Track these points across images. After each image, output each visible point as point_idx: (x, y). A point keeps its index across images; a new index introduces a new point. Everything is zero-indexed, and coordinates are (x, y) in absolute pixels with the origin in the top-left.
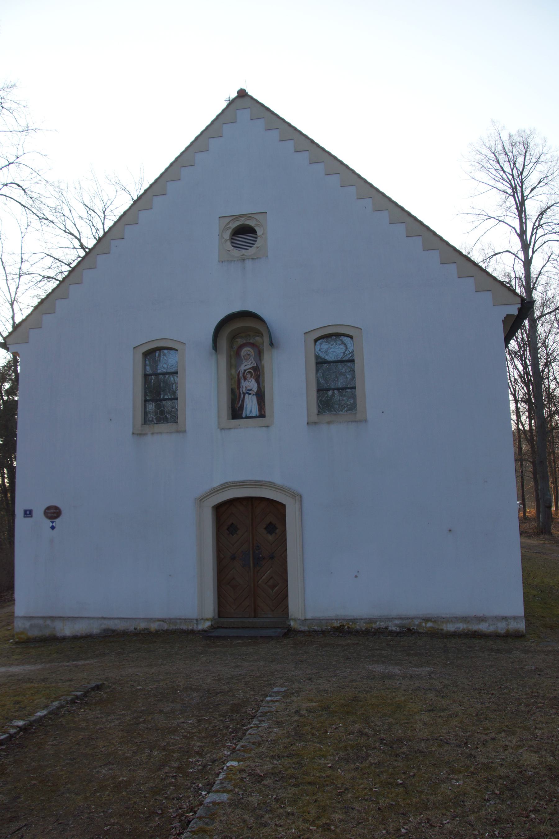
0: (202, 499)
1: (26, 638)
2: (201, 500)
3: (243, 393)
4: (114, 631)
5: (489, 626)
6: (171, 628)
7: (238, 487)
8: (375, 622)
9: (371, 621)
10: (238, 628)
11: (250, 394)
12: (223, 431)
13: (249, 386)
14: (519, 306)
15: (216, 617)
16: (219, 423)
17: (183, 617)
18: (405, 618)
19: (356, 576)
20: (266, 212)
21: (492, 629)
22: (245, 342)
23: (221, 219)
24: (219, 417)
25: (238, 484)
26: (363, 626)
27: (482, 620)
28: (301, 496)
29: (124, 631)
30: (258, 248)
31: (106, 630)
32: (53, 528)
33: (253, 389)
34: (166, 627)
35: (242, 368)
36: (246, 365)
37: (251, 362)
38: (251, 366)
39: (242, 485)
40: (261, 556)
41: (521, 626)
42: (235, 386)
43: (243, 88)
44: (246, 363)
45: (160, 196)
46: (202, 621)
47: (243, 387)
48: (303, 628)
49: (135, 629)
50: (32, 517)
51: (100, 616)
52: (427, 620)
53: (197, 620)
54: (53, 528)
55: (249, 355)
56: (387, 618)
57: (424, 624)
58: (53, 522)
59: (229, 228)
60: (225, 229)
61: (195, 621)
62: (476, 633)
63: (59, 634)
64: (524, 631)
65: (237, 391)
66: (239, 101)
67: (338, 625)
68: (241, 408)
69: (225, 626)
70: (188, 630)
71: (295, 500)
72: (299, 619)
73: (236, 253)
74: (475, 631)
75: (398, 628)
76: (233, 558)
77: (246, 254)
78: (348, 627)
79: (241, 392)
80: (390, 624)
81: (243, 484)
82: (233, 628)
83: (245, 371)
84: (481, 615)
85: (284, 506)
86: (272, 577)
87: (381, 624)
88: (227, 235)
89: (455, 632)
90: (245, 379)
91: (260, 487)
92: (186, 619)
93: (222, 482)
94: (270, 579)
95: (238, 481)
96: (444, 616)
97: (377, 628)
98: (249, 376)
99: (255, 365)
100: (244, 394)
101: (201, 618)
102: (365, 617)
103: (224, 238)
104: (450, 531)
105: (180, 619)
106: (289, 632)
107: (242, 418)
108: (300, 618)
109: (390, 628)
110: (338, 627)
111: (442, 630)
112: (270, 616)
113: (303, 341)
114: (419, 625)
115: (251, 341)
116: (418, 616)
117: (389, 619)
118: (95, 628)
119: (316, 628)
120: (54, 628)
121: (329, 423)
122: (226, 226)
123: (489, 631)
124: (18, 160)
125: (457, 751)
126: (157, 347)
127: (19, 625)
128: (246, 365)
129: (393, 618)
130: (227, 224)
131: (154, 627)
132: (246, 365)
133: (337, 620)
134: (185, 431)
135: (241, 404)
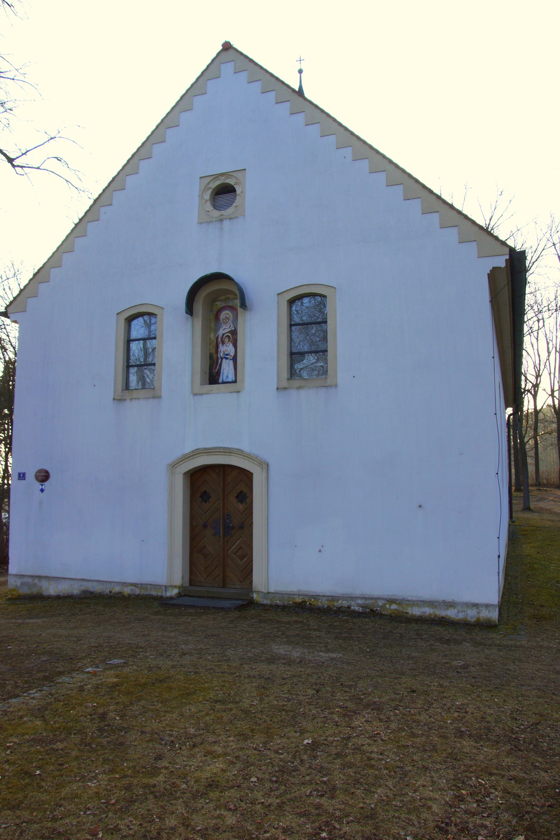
0: (174, 466)
1: (17, 595)
2: (173, 467)
3: (221, 357)
4: (92, 593)
5: (458, 612)
6: (142, 593)
7: (208, 454)
8: (338, 601)
9: (333, 598)
10: (203, 597)
11: (227, 359)
12: (196, 397)
13: (227, 351)
14: (507, 257)
15: (187, 584)
16: (192, 389)
17: (154, 583)
18: (369, 598)
19: (320, 551)
20: (245, 169)
21: (461, 616)
22: (224, 305)
23: (202, 179)
24: (192, 382)
25: (208, 451)
26: (323, 603)
27: (451, 606)
28: (268, 465)
29: (100, 593)
30: (236, 207)
31: (85, 592)
32: (42, 490)
33: (230, 354)
34: (137, 591)
35: (221, 332)
36: (224, 329)
37: (229, 325)
38: (229, 330)
39: (213, 452)
40: (231, 525)
41: (494, 615)
42: (213, 351)
43: (227, 40)
44: (224, 327)
45: (146, 160)
46: (170, 588)
47: (220, 351)
48: (265, 602)
49: (110, 592)
50: (25, 479)
51: (80, 577)
52: (392, 601)
53: (166, 586)
54: (42, 490)
55: (228, 318)
56: (350, 597)
57: (388, 606)
58: (42, 485)
59: (209, 188)
60: (206, 189)
61: (164, 588)
62: (443, 620)
63: (45, 593)
64: (497, 621)
65: (215, 356)
66: (224, 54)
67: (300, 601)
68: (218, 373)
69: (192, 595)
70: (157, 596)
71: (262, 468)
72: (262, 592)
73: (216, 213)
74: (443, 617)
75: (360, 608)
76: (205, 526)
77: (224, 214)
78: (310, 604)
79: (219, 356)
80: (353, 603)
81: (213, 450)
82: (199, 597)
83: (223, 335)
84: (450, 600)
85: (252, 474)
86: (241, 548)
87: (344, 602)
88: (207, 196)
89: (421, 616)
90: (223, 343)
91: (228, 454)
92: (156, 585)
93: (193, 449)
94: (239, 550)
95: (211, 448)
96: (410, 598)
97: (338, 606)
98: (227, 340)
99: (233, 329)
100: (222, 359)
101: (169, 585)
102: (328, 594)
103: (204, 199)
104: (420, 506)
105: (151, 585)
106: (251, 603)
107: (218, 383)
108: (263, 591)
109: (352, 608)
110: (299, 603)
111: (407, 613)
112: (238, 587)
113: (276, 302)
114: (383, 606)
115: (230, 304)
116: (383, 597)
117: (353, 598)
118: (75, 589)
119: (278, 602)
120: (41, 587)
121: (299, 388)
122: (206, 186)
123: (458, 618)
124: (59, 135)
125: (219, 735)
126: (139, 313)
127: (13, 582)
128: (224, 329)
129: (356, 597)
130: (208, 184)
131: (127, 591)
132: (224, 329)
133: (299, 595)
134: (159, 397)
135: (218, 369)
